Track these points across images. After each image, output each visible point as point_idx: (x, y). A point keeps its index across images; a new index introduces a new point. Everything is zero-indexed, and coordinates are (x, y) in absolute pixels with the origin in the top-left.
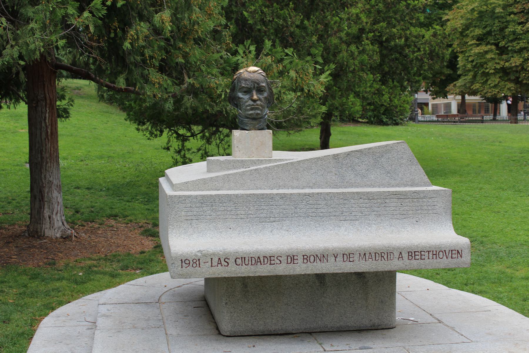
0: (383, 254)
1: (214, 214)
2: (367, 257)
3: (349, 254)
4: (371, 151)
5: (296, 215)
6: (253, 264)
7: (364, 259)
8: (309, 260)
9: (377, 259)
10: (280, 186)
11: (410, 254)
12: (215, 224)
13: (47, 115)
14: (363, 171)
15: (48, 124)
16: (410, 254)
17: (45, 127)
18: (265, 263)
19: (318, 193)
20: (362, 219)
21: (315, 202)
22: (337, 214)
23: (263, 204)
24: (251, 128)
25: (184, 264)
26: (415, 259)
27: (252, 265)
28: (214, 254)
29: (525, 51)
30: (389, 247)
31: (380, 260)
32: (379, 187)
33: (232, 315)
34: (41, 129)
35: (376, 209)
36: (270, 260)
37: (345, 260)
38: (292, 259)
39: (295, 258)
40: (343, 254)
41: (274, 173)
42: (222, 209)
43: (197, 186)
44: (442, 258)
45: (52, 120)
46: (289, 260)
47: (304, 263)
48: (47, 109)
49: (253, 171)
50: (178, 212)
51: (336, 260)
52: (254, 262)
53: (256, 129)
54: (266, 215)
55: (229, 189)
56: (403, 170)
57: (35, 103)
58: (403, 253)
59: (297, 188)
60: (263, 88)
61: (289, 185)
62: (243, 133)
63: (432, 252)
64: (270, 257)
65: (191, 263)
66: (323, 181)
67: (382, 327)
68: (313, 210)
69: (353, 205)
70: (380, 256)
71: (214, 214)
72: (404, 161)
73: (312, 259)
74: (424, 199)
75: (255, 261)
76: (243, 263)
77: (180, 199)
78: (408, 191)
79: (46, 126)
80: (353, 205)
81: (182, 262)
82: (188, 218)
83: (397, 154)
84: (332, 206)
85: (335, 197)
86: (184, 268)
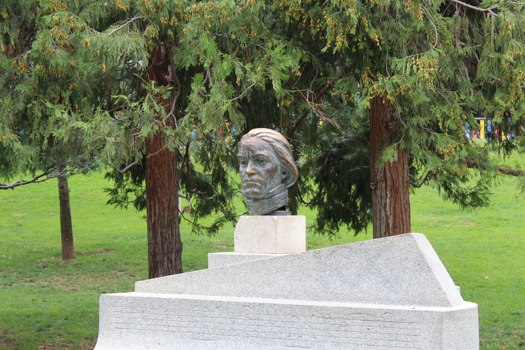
1: (145, 323)
5: (234, 333)
10: (248, 293)
12: (144, 337)
13: (388, 201)
14: (352, 277)
15: (389, 213)
17: (385, 217)
19: (260, 304)
20: (315, 346)
21: (257, 316)
22: (283, 336)
23: (196, 315)
32: (374, 302)
34: (380, 220)
35: (333, 333)
41: (241, 274)
42: (152, 317)
43: (158, 287)
45: (395, 207)
48: (388, 193)
49: (218, 271)
50: (110, 318)
53: (259, 213)
55: (192, 293)
56: (408, 278)
57: (373, 185)
59: (269, 296)
60: (262, 157)
61: (259, 292)
66: (300, 288)
68: (254, 328)
69: (303, 325)
71: (145, 323)
74: (401, 324)
77: (112, 301)
78: (378, 309)
79: (387, 217)
80: (303, 325)
82: (119, 326)
84: (277, 324)
85: (280, 311)
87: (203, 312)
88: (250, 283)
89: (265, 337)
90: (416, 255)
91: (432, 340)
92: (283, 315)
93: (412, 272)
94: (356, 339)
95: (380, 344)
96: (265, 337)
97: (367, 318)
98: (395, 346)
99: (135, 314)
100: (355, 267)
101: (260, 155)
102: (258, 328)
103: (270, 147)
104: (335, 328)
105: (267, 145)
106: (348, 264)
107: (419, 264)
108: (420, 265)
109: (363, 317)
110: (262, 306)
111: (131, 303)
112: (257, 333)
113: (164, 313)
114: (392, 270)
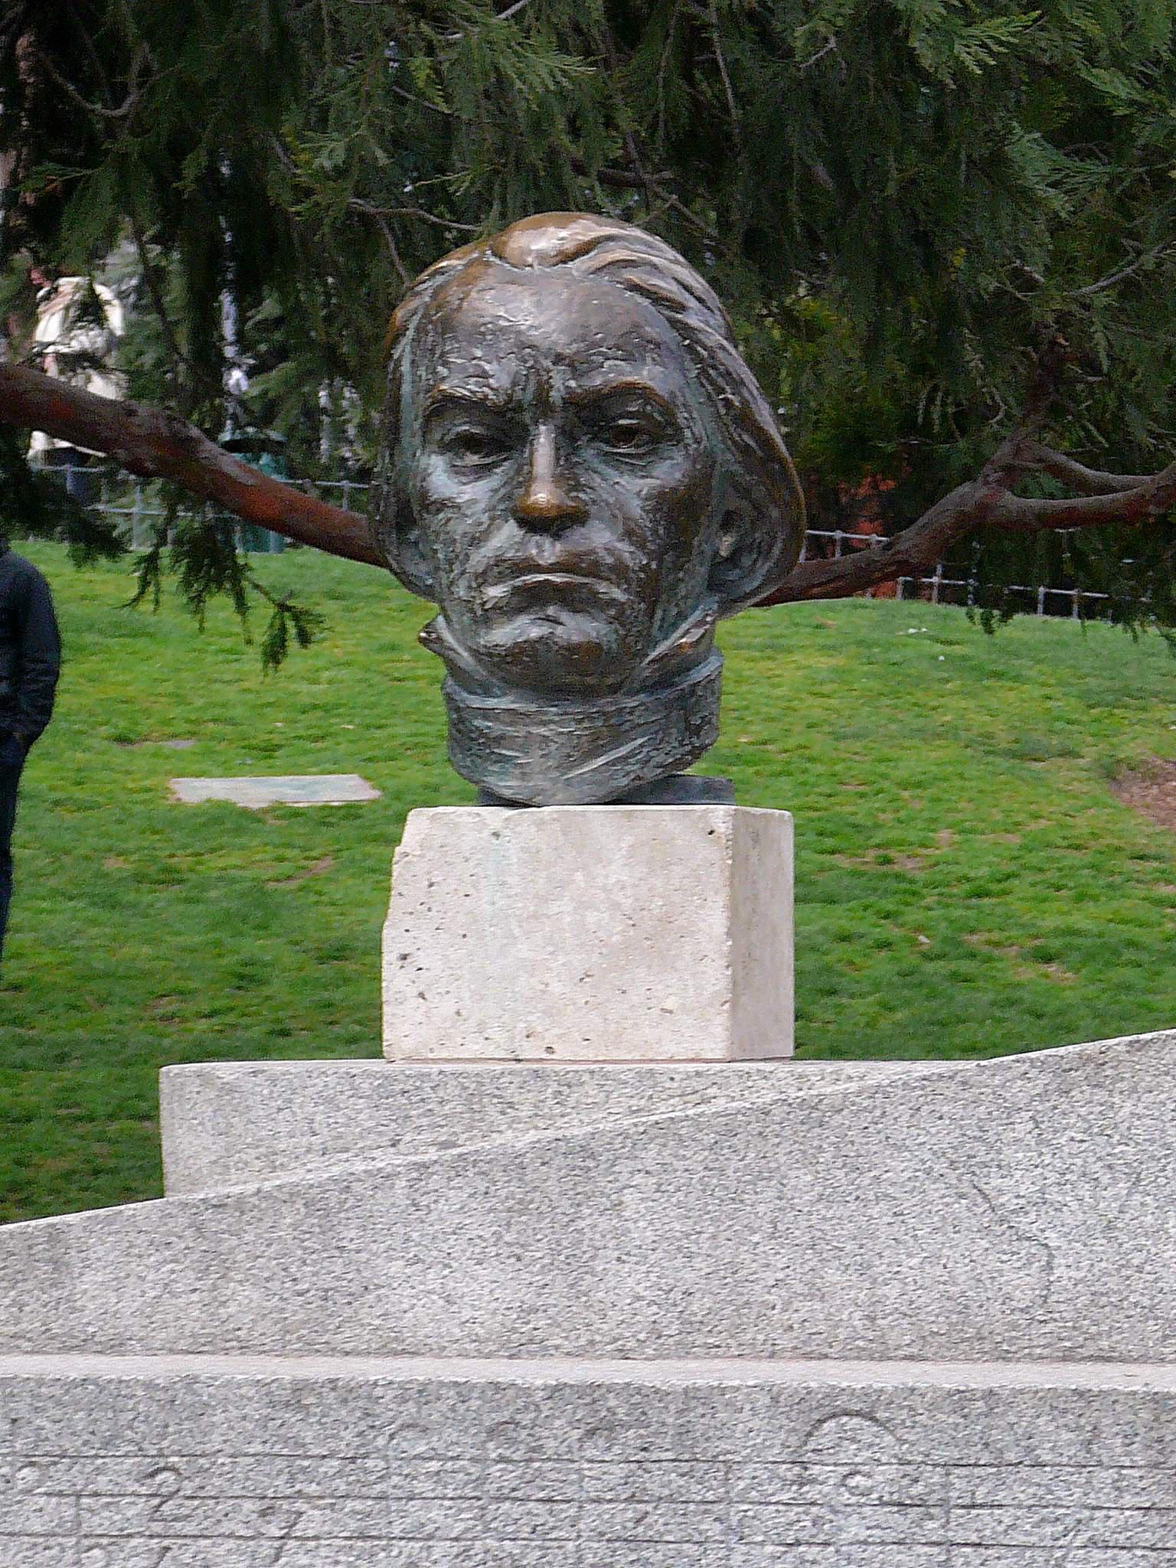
23: (422, 1486)
24: (538, 782)
66: (1113, 1283)
84: (1099, 1527)
87: (475, 1470)
88: (697, 1262)
92: (1156, 1465)
101: (630, 390)
103: (670, 336)
105: (657, 328)
113: (136, 1487)
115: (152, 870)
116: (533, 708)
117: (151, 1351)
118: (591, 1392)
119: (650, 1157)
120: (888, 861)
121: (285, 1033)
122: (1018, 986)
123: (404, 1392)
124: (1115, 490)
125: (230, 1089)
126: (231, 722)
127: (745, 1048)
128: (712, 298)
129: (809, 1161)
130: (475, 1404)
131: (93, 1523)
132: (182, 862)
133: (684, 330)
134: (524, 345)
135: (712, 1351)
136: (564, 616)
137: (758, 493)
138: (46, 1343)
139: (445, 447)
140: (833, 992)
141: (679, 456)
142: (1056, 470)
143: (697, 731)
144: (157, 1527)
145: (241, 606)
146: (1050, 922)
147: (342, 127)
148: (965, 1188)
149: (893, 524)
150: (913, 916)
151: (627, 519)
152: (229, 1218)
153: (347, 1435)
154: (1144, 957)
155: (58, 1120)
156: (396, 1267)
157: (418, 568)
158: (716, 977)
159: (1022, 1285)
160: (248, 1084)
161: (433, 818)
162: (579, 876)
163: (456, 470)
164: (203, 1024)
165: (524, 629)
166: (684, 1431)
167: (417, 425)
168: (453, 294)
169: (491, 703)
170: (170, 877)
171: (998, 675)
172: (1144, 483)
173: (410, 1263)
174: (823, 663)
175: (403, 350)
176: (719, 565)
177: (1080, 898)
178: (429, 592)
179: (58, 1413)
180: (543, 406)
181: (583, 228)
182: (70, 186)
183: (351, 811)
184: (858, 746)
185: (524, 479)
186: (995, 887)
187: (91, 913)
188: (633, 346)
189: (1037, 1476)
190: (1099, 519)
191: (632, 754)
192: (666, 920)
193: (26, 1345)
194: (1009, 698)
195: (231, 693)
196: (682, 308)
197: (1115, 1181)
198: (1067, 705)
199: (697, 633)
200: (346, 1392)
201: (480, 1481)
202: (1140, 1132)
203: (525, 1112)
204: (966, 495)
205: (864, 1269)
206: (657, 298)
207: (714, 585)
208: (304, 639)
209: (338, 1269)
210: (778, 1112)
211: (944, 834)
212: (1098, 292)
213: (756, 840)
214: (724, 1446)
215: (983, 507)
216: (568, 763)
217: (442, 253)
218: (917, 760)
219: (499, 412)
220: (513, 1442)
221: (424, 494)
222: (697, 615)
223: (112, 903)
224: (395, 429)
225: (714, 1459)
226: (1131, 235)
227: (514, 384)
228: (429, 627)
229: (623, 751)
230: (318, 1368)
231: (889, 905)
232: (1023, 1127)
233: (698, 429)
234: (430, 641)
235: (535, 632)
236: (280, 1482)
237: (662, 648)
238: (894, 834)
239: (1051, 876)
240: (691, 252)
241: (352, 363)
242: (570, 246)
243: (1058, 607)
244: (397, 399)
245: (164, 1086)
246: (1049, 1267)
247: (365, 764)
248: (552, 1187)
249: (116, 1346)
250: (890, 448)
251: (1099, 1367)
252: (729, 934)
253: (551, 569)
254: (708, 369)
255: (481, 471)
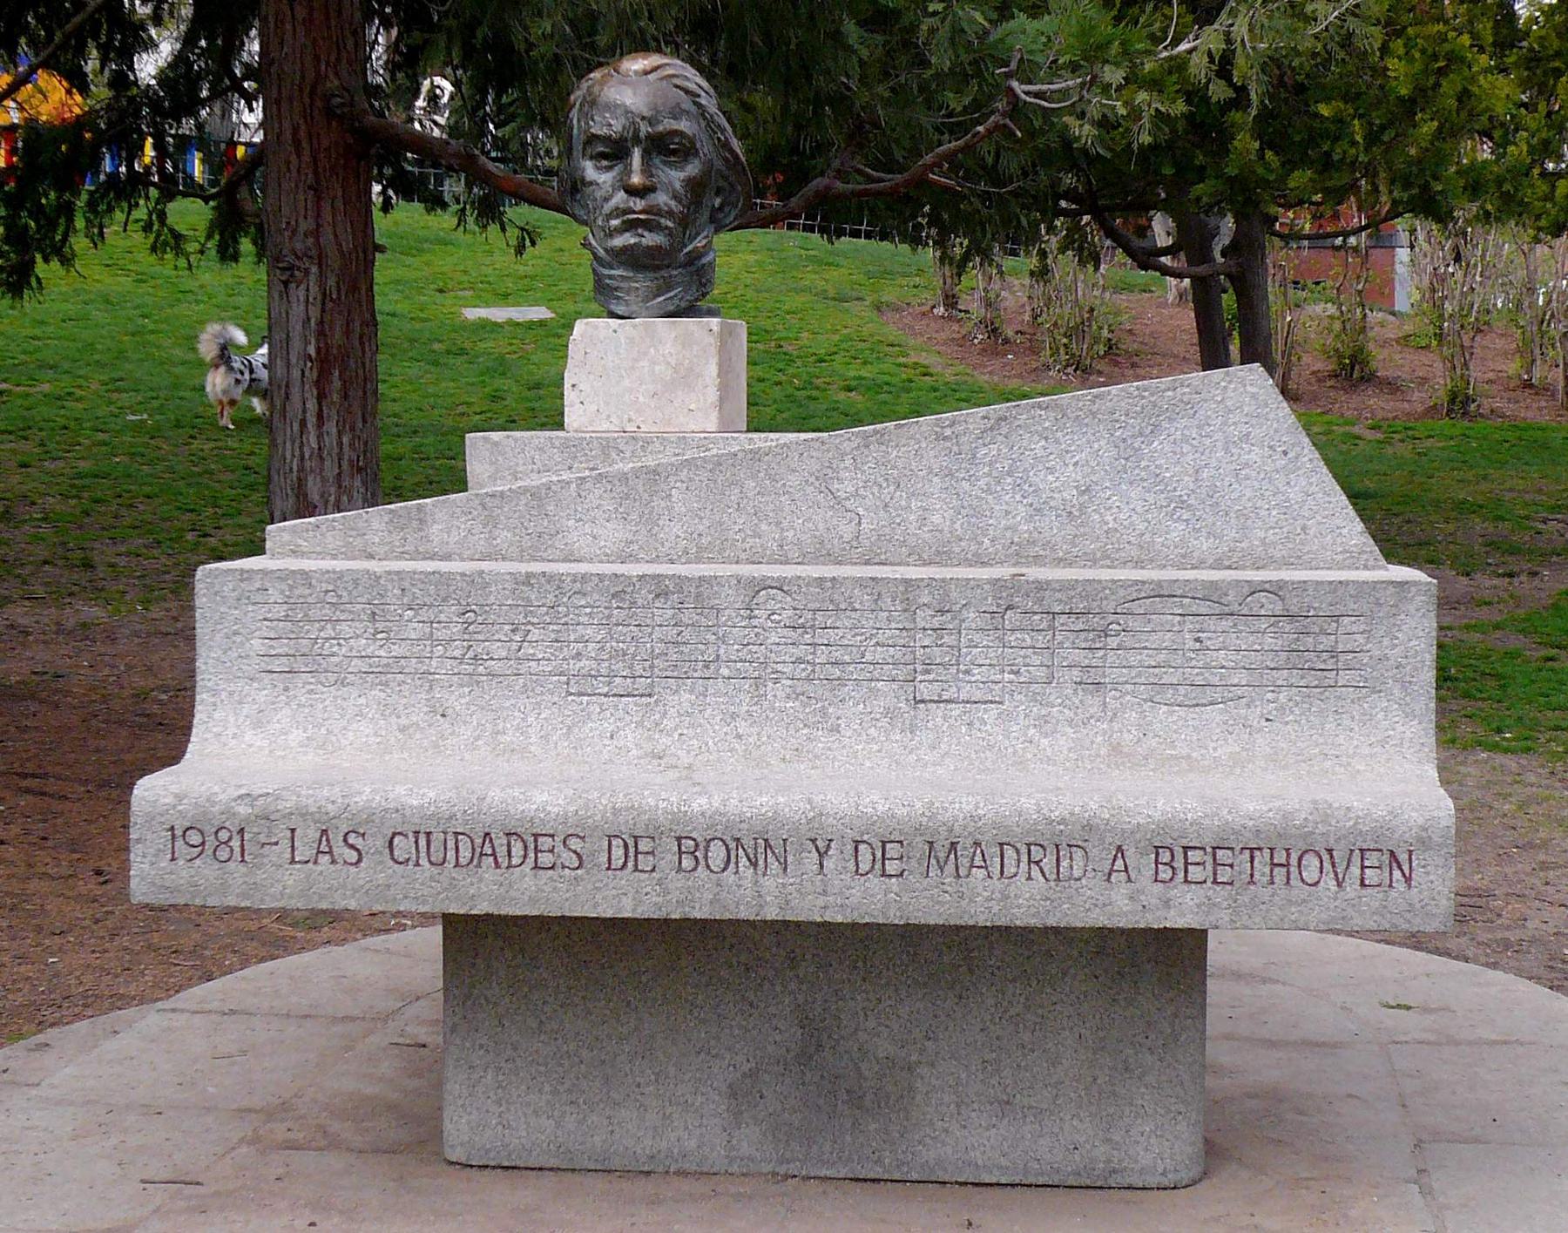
0: (1037, 853)
1: (382, 653)
2: (964, 862)
3: (884, 843)
4: (797, 427)
5: (725, 671)
6: (463, 861)
7: (950, 867)
8: (702, 862)
9: (1010, 869)
11: (1165, 857)
12: (383, 695)
16: (1165, 857)
18: (515, 861)
23: (583, 619)
24: (634, 308)
25: (179, 843)
26: (1186, 881)
27: (457, 865)
28: (304, 815)
29: (243, 193)
30: (1063, 821)
31: (1022, 878)
33: (475, 1076)
36: (536, 850)
37: (864, 867)
38: (632, 850)
39: (644, 846)
40: (857, 843)
44: (1316, 884)
46: (618, 853)
47: (680, 869)
51: (821, 866)
52: (465, 854)
54: (594, 664)
58: (1130, 853)
62: (596, 328)
63: (1267, 852)
64: (536, 836)
65: (211, 842)
66: (887, 530)
67: (1127, 1181)
70: (1025, 858)
72: (1255, 455)
73: (717, 853)
75: (473, 849)
76: (423, 854)
81: (173, 837)
83: (1224, 423)
84: (880, 638)
86: (181, 862)
87: (607, 612)
89: (839, 679)
90: (1275, 425)
91: (1404, 661)
92: (905, 610)
93: (1262, 476)
94: (1157, 670)
95: (1236, 681)
96: (839, 679)
97: (1194, 609)
98: (1285, 683)
99: (344, 627)
100: (1076, 464)
102: (814, 653)
103: (693, 109)
104: (1086, 640)
105: (687, 104)
106: (1052, 457)
107: (1285, 453)
108: (1289, 456)
109: (1182, 606)
110: (829, 584)
111: (327, 592)
112: (810, 668)
114: (1197, 471)
115: (454, 349)
116: (631, 274)
117: (463, 560)
118: (658, 577)
119: (684, 474)
120: (781, 347)
121: (514, 421)
122: (837, 402)
123: (575, 578)
124: (884, 181)
125: (496, 444)
126: (489, 283)
127: (725, 427)
128: (712, 91)
129: (753, 477)
130: (606, 583)
131: (438, 634)
132: (467, 345)
133: (699, 105)
134: (627, 111)
135: (711, 560)
136: (646, 233)
137: (733, 179)
138: (416, 555)
139: (591, 158)
140: (757, 404)
141: (696, 162)
142: (859, 172)
143: (704, 285)
144: (466, 637)
145: (503, 229)
146: (852, 374)
147: (549, 16)
148: (823, 489)
149: (783, 196)
150: (791, 371)
151: (674, 190)
152: (497, 501)
153: (551, 597)
154: (892, 389)
155: (413, 459)
156: (571, 523)
157: (581, 213)
158: (712, 395)
159: (847, 531)
160: (505, 442)
161: (587, 324)
162: (652, 350)
163: (598, 168)
164: (478, 417)
165: (628, 239)
166: (698, 595)
167: (580, 148)
168: (596, 89)
169: (613, 272)
170: (462, 352)
171: (830, 264)
172: (898, 178)
173: (577, 521)
174: (752, 258)
175: (574, 114)
176: (714, 211)
177: (865, 363)
178: (585, 223)
179: (422, 586)
180: (636, 140)
181: (655, 60)
182: (426, 42)
183: (542, 323)
184: (766, 295)
185: (628, 171)
186: (827, 358)
187: (427, 367)
188: (677, 113)
189: (853, 614)
190: (878, 194)
191: (676, 296)
192: (691, 369)
193: (407, 556)
194: (834, 274)
195: (490, 271)
196: (699, 96)
197: (888, 486)
198: (861, 278)
199: (704, 242)
200: (549, 578)
201: (609, 617)
202: (900, 464)
203: (628, 454)
204: (818, 183)
205: (778, 524)
206: (687, 92)
207: (712, 220)
208: (533, 243)
209: (546, 524)
210: (740, 455)
211: (805, 335)
212: (882, 90)
213: (730, 334)
214: (717, 602)
215: (828, 188)
216: (647, 299)
217: (591, 71)
218: (798, 301)
219: (616, 142)
220: (623, 600)
221: (583, 179)
222: (705, 233)
223: (436, 363)
224: (570, 149)
225: (712, 608)
226: (894, 68)
227: (624, 128)
228: (585, 239)
229: (672, 294)
230: (537, 567)
231: (781, 366)
232: (848, 462)
233: (706, 151)
234: (586, 245)
235: (632, 241)
236: (521, 617)
237: (690, 248)
238: (784, 334)
239: (853, 353)
240: (701, 69)
241: (552, 121)
242: (648, 68)
243: (856, 234)
244: (571, 136)
245: (467, 442)
246: (860, 523)
247: (548, 303)
248: (641, 489)
249: (447, 557)
250: (785, 161)
251: (881, 567)
252: (719, 376)
253: (640, 212)
254: (710, 122)
255: (609, 168)
